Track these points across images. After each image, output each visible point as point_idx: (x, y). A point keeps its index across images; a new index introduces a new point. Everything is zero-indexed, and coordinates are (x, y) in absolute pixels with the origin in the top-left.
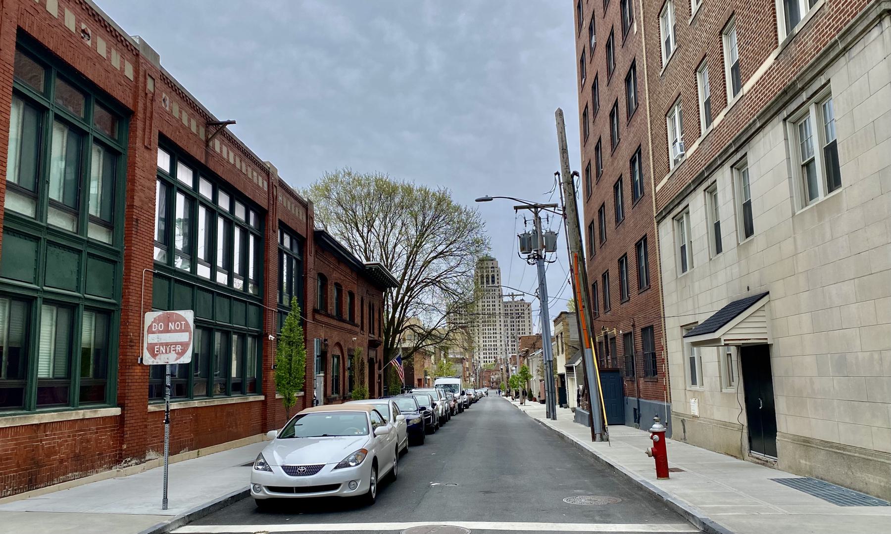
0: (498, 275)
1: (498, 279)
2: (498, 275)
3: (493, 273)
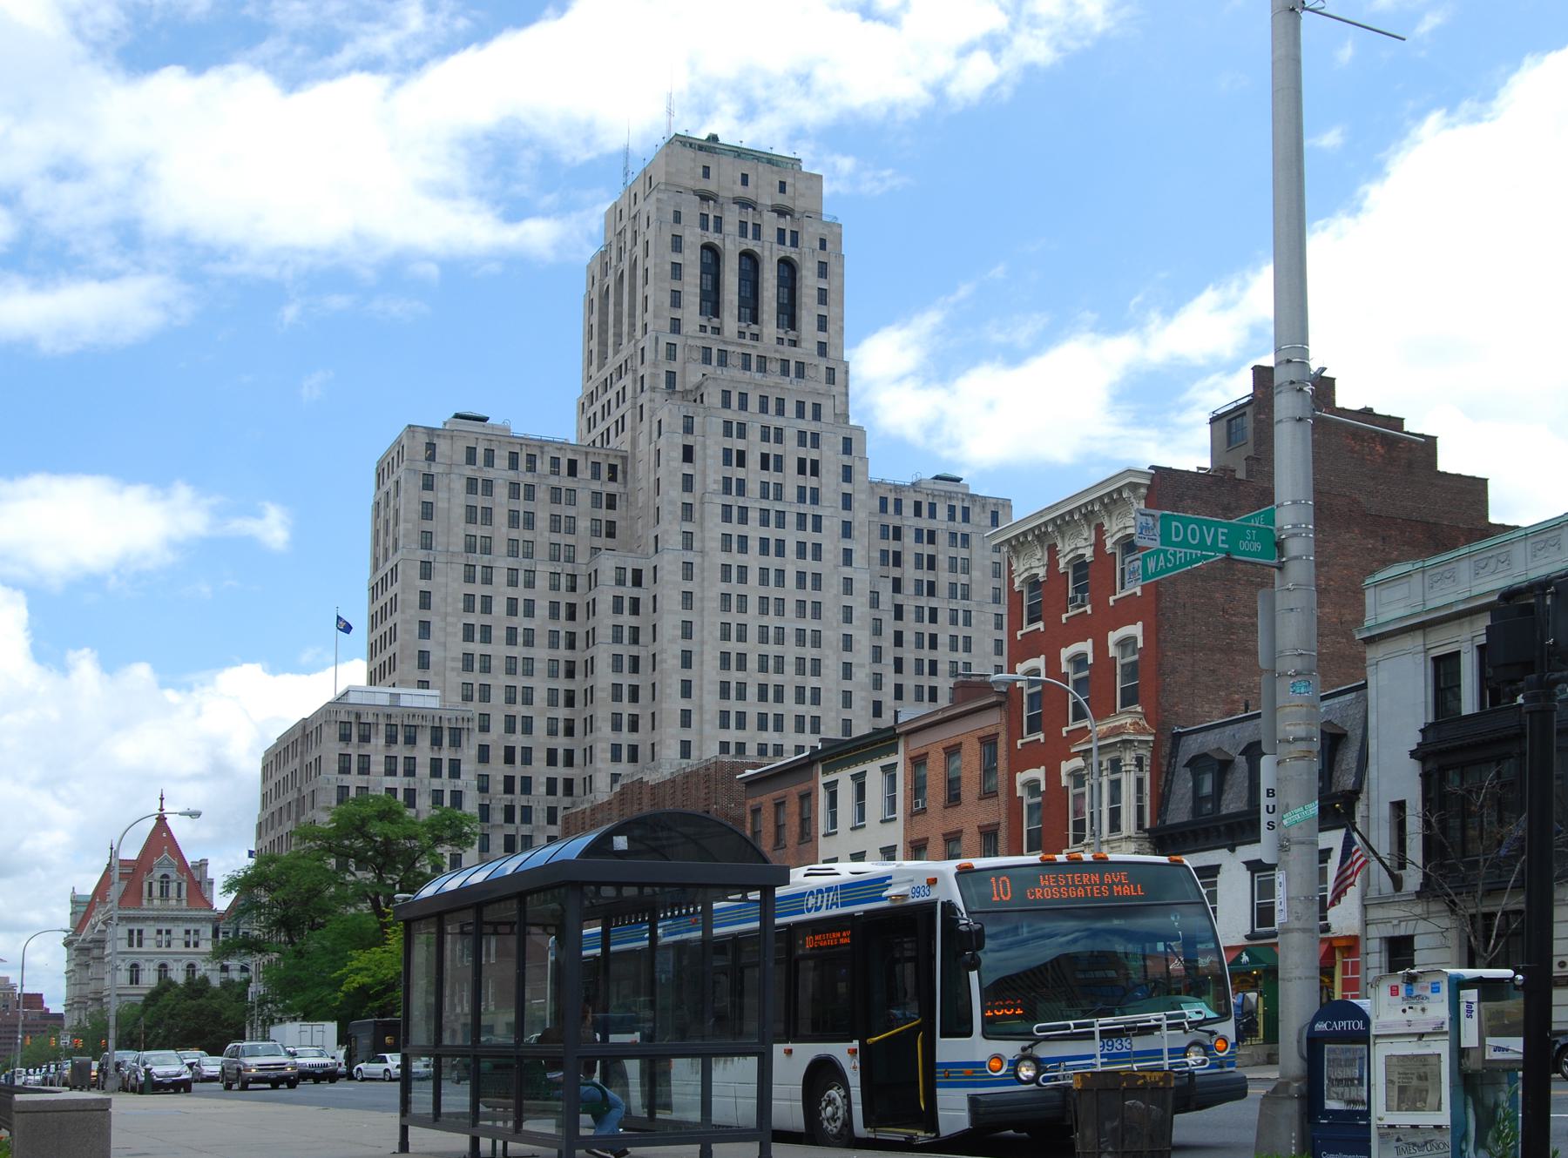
0: (823, 269)
1: (823, 296)
2: (823, 269)
3: (787, 251)
